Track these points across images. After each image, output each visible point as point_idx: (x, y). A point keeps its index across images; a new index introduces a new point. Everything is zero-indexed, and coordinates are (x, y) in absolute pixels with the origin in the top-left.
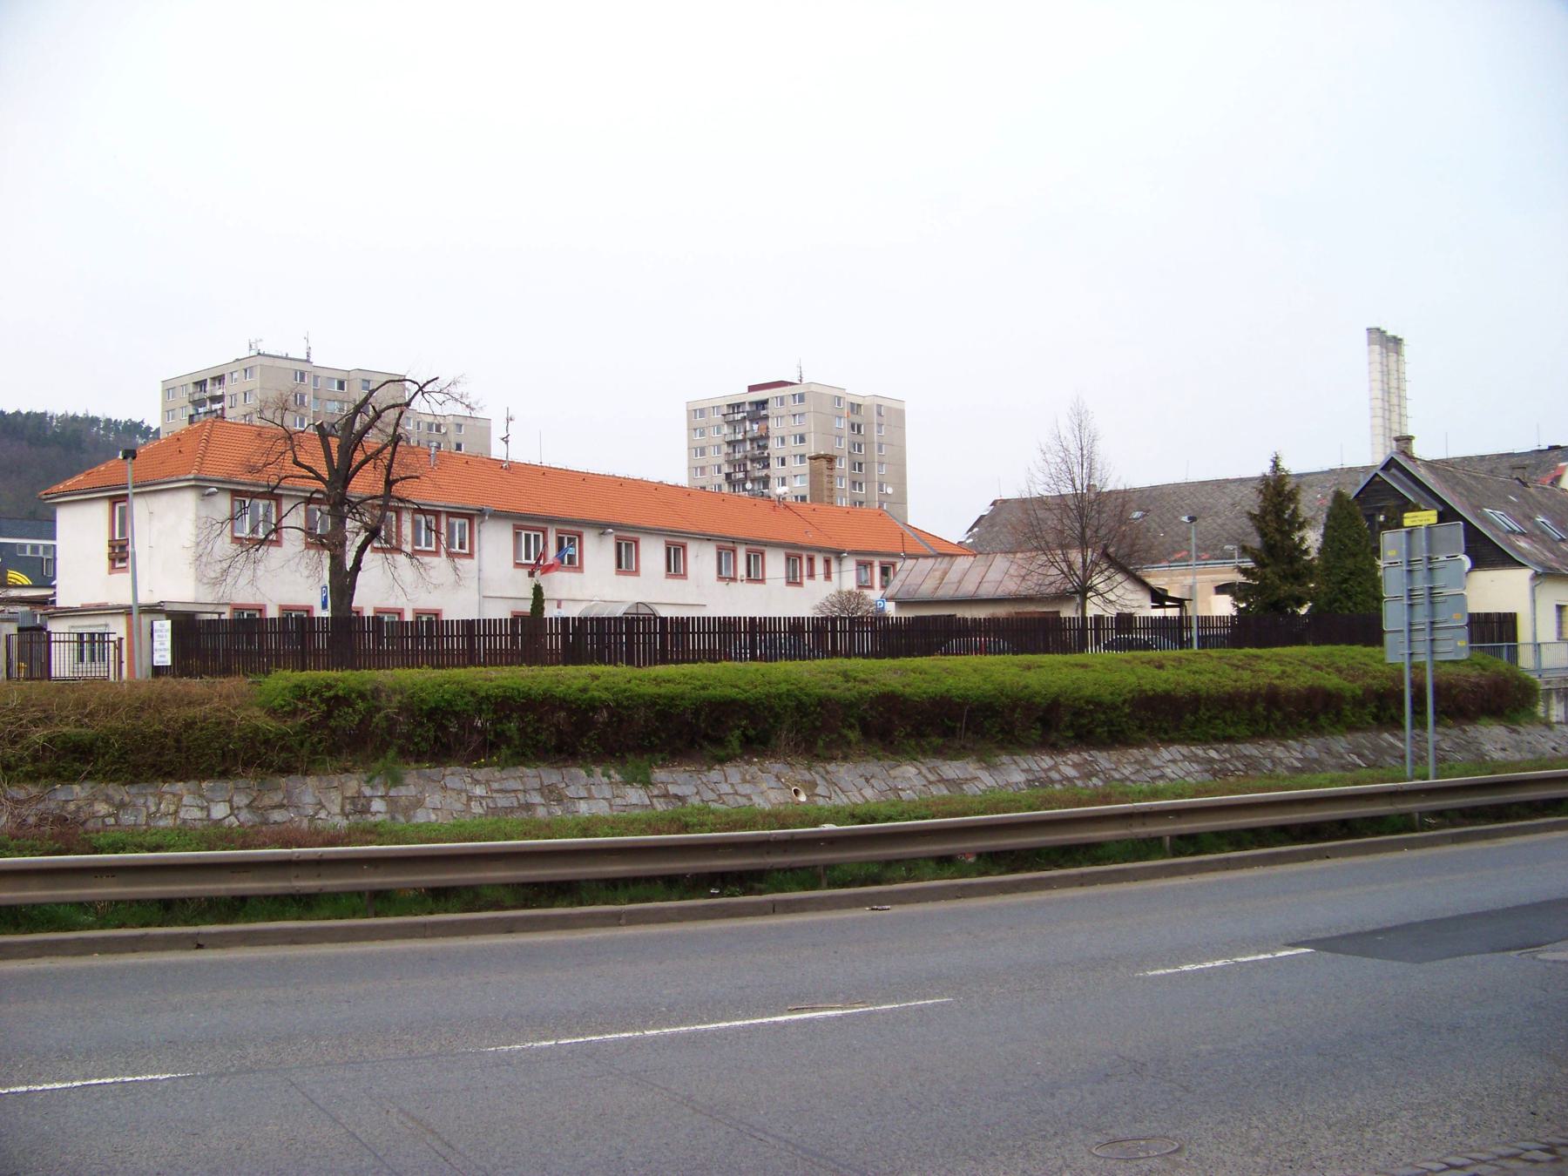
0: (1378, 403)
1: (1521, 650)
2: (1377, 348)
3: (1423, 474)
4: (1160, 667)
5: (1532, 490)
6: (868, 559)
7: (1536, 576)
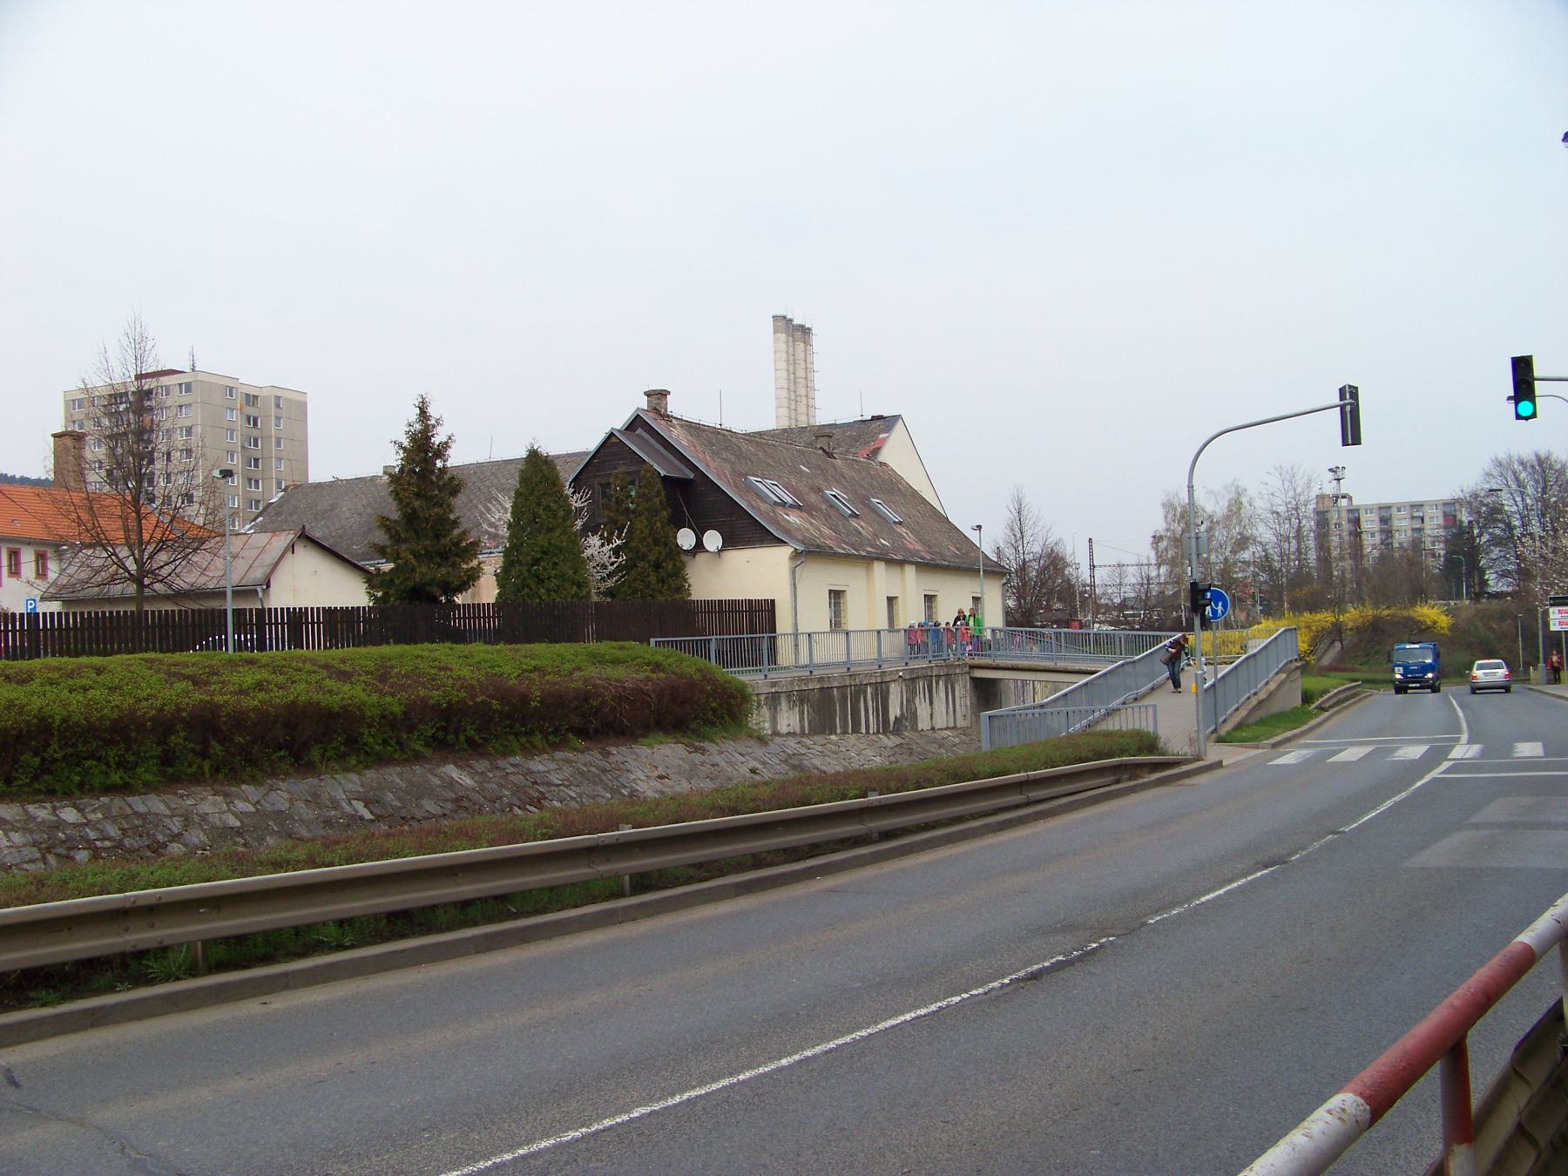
0: (784, 393)
1: (779, 642)
2: (783, 336)
3: (677, 437)
4: (345, 676)
5: (838, 462)
6: (17, 546)
7: (797, 555)
